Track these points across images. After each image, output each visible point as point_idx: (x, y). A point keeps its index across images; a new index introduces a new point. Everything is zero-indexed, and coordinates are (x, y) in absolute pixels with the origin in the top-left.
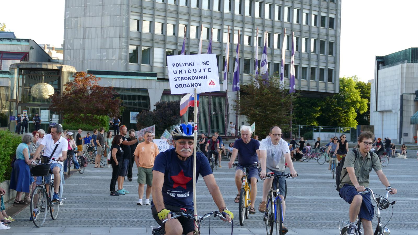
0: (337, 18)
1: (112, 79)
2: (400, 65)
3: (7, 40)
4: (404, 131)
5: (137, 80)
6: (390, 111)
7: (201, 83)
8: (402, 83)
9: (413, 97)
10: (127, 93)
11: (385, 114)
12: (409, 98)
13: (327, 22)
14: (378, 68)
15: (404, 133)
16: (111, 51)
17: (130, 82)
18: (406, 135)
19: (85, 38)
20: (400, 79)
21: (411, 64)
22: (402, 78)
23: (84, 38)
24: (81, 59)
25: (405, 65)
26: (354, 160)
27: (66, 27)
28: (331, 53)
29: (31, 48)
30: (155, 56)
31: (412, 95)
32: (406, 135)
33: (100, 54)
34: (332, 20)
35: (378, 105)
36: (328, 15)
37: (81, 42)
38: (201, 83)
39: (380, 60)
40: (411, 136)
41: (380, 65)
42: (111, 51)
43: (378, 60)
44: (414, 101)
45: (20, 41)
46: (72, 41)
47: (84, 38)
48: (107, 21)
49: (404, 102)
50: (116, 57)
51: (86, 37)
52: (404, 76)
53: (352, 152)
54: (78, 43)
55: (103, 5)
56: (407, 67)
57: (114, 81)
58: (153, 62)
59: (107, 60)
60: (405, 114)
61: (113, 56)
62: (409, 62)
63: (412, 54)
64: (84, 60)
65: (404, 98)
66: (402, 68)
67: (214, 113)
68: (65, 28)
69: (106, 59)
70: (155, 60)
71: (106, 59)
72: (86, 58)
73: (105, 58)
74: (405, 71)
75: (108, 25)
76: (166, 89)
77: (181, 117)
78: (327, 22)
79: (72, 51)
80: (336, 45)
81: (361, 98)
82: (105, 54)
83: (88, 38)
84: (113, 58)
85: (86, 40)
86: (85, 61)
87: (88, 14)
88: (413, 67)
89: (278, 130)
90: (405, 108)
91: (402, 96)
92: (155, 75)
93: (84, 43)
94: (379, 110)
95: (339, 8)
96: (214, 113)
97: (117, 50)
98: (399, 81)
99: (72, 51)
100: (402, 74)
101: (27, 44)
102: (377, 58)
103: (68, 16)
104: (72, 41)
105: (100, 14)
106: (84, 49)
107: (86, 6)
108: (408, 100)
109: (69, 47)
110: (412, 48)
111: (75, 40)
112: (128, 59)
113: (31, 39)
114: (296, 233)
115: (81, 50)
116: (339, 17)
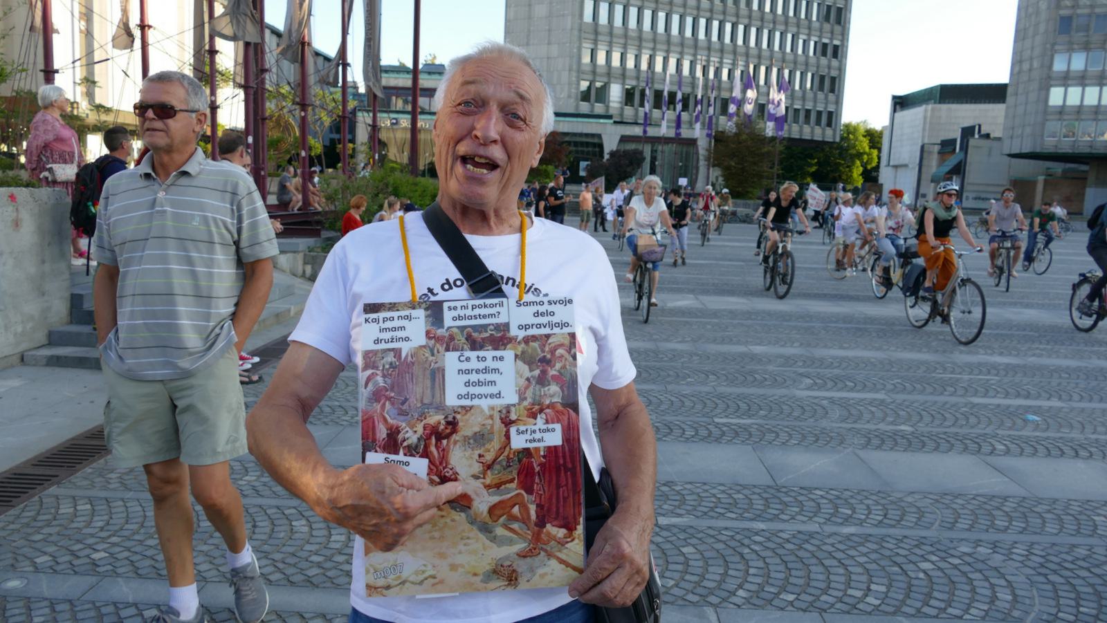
2: (924, 106)
4: (921, 191)
6: (906, 166)
8: (924, 130)
9: (937, 148)
11: (899, 170)
13: (830, 51)
25: (930, 107)
28: (832, 91)
32: (924, 196)
34: (836, 48)
41: (898, 107)
48: (555, 50)
49: (925, 155)
52: (928, 120)
55: (549, 30)
56: (933, 110)
65: (926, 148)
66: (926, 111)
74: (929, 114)
78: (830, 51)
91: (922, 147)
92: (610, 117)
97: (566, 88)
100: (925, 118)
102: (894, 97)
107: (529, 31)
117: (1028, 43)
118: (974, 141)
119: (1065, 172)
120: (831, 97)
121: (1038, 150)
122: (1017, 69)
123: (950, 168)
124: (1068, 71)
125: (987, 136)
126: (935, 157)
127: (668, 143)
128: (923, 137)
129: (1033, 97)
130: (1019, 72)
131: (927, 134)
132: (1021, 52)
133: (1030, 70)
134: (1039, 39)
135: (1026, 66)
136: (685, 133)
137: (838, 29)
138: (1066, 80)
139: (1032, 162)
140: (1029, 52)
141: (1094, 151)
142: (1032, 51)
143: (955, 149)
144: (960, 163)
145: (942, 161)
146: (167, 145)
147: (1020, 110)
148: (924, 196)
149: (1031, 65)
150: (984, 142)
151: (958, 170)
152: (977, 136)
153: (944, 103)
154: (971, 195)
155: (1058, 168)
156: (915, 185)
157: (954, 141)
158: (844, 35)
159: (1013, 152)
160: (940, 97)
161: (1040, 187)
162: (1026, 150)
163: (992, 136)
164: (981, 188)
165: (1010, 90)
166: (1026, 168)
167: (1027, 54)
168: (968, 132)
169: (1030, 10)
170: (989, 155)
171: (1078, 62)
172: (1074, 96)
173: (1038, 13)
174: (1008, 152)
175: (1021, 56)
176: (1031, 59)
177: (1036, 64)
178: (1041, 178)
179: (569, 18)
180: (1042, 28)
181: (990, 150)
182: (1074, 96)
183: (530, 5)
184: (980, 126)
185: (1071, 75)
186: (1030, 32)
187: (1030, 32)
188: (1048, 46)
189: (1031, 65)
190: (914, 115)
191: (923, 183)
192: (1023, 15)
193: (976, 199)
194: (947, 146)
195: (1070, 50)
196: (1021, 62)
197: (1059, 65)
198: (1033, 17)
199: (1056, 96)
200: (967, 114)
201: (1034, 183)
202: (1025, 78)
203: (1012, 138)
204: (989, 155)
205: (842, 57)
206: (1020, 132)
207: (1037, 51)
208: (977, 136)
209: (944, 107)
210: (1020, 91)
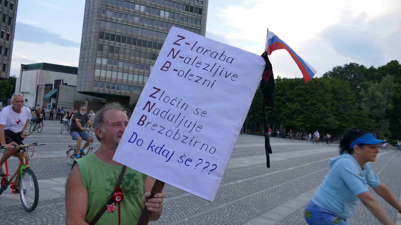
0: (12, 34)
2: (37, 70)
4: (38, 103)
6: (28, 93)
7: (178, 36)
8: (37, 79)
9: (44, 87)
11: (24, 94)
12: (41, 87)
13: (5, 36)
14: (22, 71)
15: (38, 105)
18: (39, 105)
20: (36, 77)
22: (37, 77)
25: (39, 71)
31: (44, 86)
32: (39, 105)
34: (8, 35)
35: (21, 89)
36: (6, 32)
38: (178, 36)
39: (24, 66)
41: (24, 69)
43: (23, 66)
44: (45, 89)
49: (39, 89)
52: (38, 76)
56: (40, 72)
62: (41, 69)
65: (39, 86)
66: (37, 72)
74: (39, 73)
78: (5, 36)
80: (10, 50)
81: (9, 85)
88: (43, 72)
89: (317, 131)
91: (38, 86)
94: (21, 91)
95: (13, 29)
98: (35, 78)
100: (37, 75)
102: (22, 65)
108: (41, 88)
110: (44, 63)
114: (52, 188)
116: (13, 35)
119: (93, 99)
120: (5, 58)
121: (92, 91)
122: (82, 60)
123: (51, 95)
124: (101, 64)
125: (66, 84)
130: (83, 62)
131: (38, 81)
133: (88, 61)
134: (91, 51)
135: (86, 60)
138: (101, 67)
139: (82, 94)
140: (87, 55)
141: (110, 93)
142: (88, 55)
143: (52, 88)
146: (84, 153)
149: (88, 59)
150: (64, 86)
152: (62, 84)
155: (91, 98)
156: (35, 100)
159: (81, 91)
160: (43, 68)
162: (87, 90)
163: (68, 84)
164: (64, 104)
166: (81, 97)
168: (58, 82)
169: (87, 40)
170: (67, 91)
174: (79, 91)
177: (90, 60)
184: (63, 80)
186: (88, 47)
187: (88, 47)
190: (33, 73)
192: (84, 41)
194: (48, 87)
195: (102, 57)
196: (84, 58)
198: (88, 43)
200: (53, 76)
204: (67, 91)
205: (11, 40)
206: (84, 84)
208: (62, 84)
210: (84, 69)
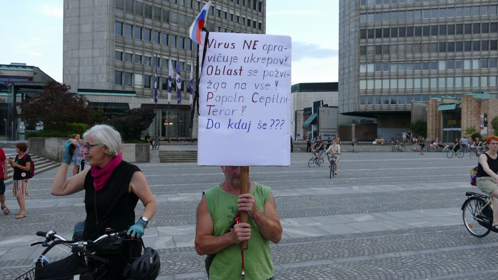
1: (98, 96)
3: (14, 67)
4: (297, 133)
5: (119, 97)
8: (294, 104)
9: (302, 112)
10: (113, 107)
12: (300, 113)
13: (252, 23)
16: (100, 75)
17: (114, 98)
19: (80, 66)
21: (300, 93)
22: (294, 101)
23: (79, 66)
24: (77, 82)
25: (296, 93)
26: (202, 195)
27: (65, 58)
28: (260, 10)
29: (35, 73)
30: (136, 80)
32: (299, 135)
33: (91, 78)
34: (260, 24)
37: (77, 69)
40: (302, 135)
42: (100, 75)
44: (303, 114)
45: (25, 68)
46: (69, 68)
47: (79, 66)
48: (97, 53)
50: (104, 80)
51: (81, 65)
52: (296, 99)
53: (155, 247)
54: (74, 70)
55: (93, 40)
56: (297, 95)
57: (100, 97)
58: (134, 85)
59: (97, 83)
60: (298, 122)
61: (102, 79)
62: (298, 92)
63: (300, 87)
64: (79, 83)
65: (297, 113)
66: (294, 95)
67: (181, 121)
68: (63, 58)
69: (97, 82)
70: (136, 83)
71: (97, 82)
72: (81, 82)
73: (96, 81)
74: (296, 97)
75: (98, 55)
76: (143, 103)
77: (64, 85)
79: (70, 76)
82: (95, 78)
83: (82, 66)
84: (102, 81)
85: (81, 67)
86: (80, 84)
87: (81, 47)
88: (301, 95)
90: (298, 119)
91: (296, 112)
92: (134, 92)
93: (78, 70)
96: (181, 121)
97: (105, 76)
99: (70, 76)
100: (294, 99)
101: (32, 70)
103: (65, 50)
104: (69, 68)
105: (91, 47)
106: (79, 74)
107: (79, 41)
108: (299, 114)
109: (67, 73)
111: (72, 67)
112: (114, 82)
113: (35, 66)
115: (77, 76)
117: (346, 60)
118: (321, 108)
119: (362, 121)
122: (342, 72)
123: (311, 121)
124: (367, 73)
125: (327, 106)
126: (302, 116)
127: (173, 108)
128: (294, 108)
129: (352, 85)
130: (343, 74)
131: (296, 106)
132: (343, 64)
134: (351, 58)
135: (347, 71)
136: (184, 102)
137: (260, 14)
138: (366, 77)
140: (347, 64)
141: (382, 111)
143: (311, 113)
144: (316, 118)
145: (305, 119)
147: (346, 91)
148: (299, 135)
149: (349, 70)
151: (315, 122)
152: (321, 106)
153: (302, 92)
154: (323, 134)
155: (358, 119)
157: (311, 108)
158: (263, 16)
159: (344, 112)
160: (300, 89)
161: (353, 129)
165: (339, 84)
167: (346, 65)
168: (317, 104)
169: (346, 44)
170: (329, 114)
171: (371, 68)
172: (371, 85)
173: (350, 45)
175: (344, 66)
176: (349, 67)
177: (351, 70)
178: (354, 125)
179: (106, 32)
180: (353, 52)
181: (329, 112)
182: (371, 85)
183: (79, 25)
184: (322, 101)
185: (368, 74)
186: (347, 54)
187: (347, 54)
188: (357, 60)
189: (349, 70)
191: (298, 129)
192: (342, 46)
193: (324, 135)
194: (307, 111)
195: (366, 63)
196: (344, 69)
197: (363, 70)
198: (348, 48)
199: (363, 85)
200: (312, 97)
201: (351, 127)
202: (347, 76)
203: (343, 105)
204: (329, 114)
207: (352, 63)
208: (321, 106)
209: (302, 93)
210: (345, 83)
